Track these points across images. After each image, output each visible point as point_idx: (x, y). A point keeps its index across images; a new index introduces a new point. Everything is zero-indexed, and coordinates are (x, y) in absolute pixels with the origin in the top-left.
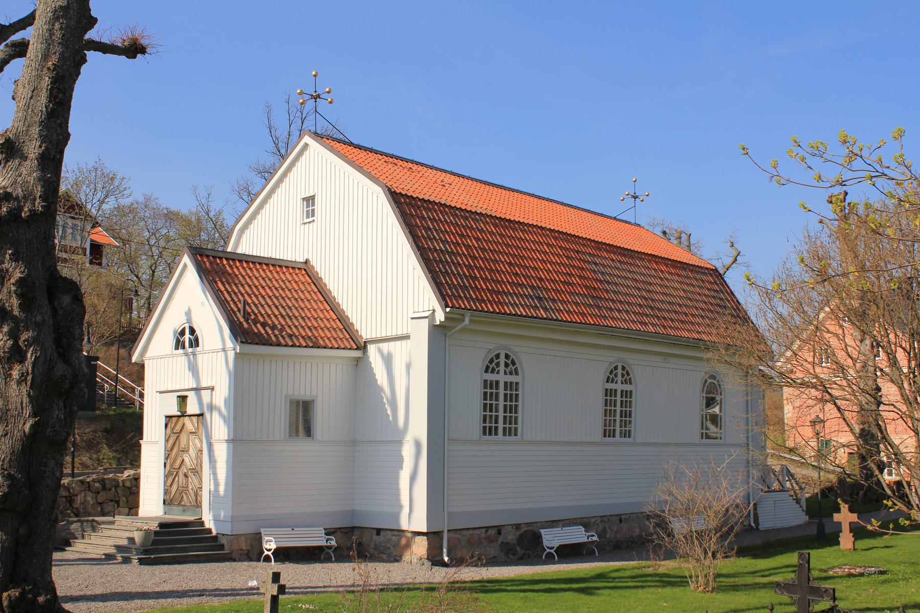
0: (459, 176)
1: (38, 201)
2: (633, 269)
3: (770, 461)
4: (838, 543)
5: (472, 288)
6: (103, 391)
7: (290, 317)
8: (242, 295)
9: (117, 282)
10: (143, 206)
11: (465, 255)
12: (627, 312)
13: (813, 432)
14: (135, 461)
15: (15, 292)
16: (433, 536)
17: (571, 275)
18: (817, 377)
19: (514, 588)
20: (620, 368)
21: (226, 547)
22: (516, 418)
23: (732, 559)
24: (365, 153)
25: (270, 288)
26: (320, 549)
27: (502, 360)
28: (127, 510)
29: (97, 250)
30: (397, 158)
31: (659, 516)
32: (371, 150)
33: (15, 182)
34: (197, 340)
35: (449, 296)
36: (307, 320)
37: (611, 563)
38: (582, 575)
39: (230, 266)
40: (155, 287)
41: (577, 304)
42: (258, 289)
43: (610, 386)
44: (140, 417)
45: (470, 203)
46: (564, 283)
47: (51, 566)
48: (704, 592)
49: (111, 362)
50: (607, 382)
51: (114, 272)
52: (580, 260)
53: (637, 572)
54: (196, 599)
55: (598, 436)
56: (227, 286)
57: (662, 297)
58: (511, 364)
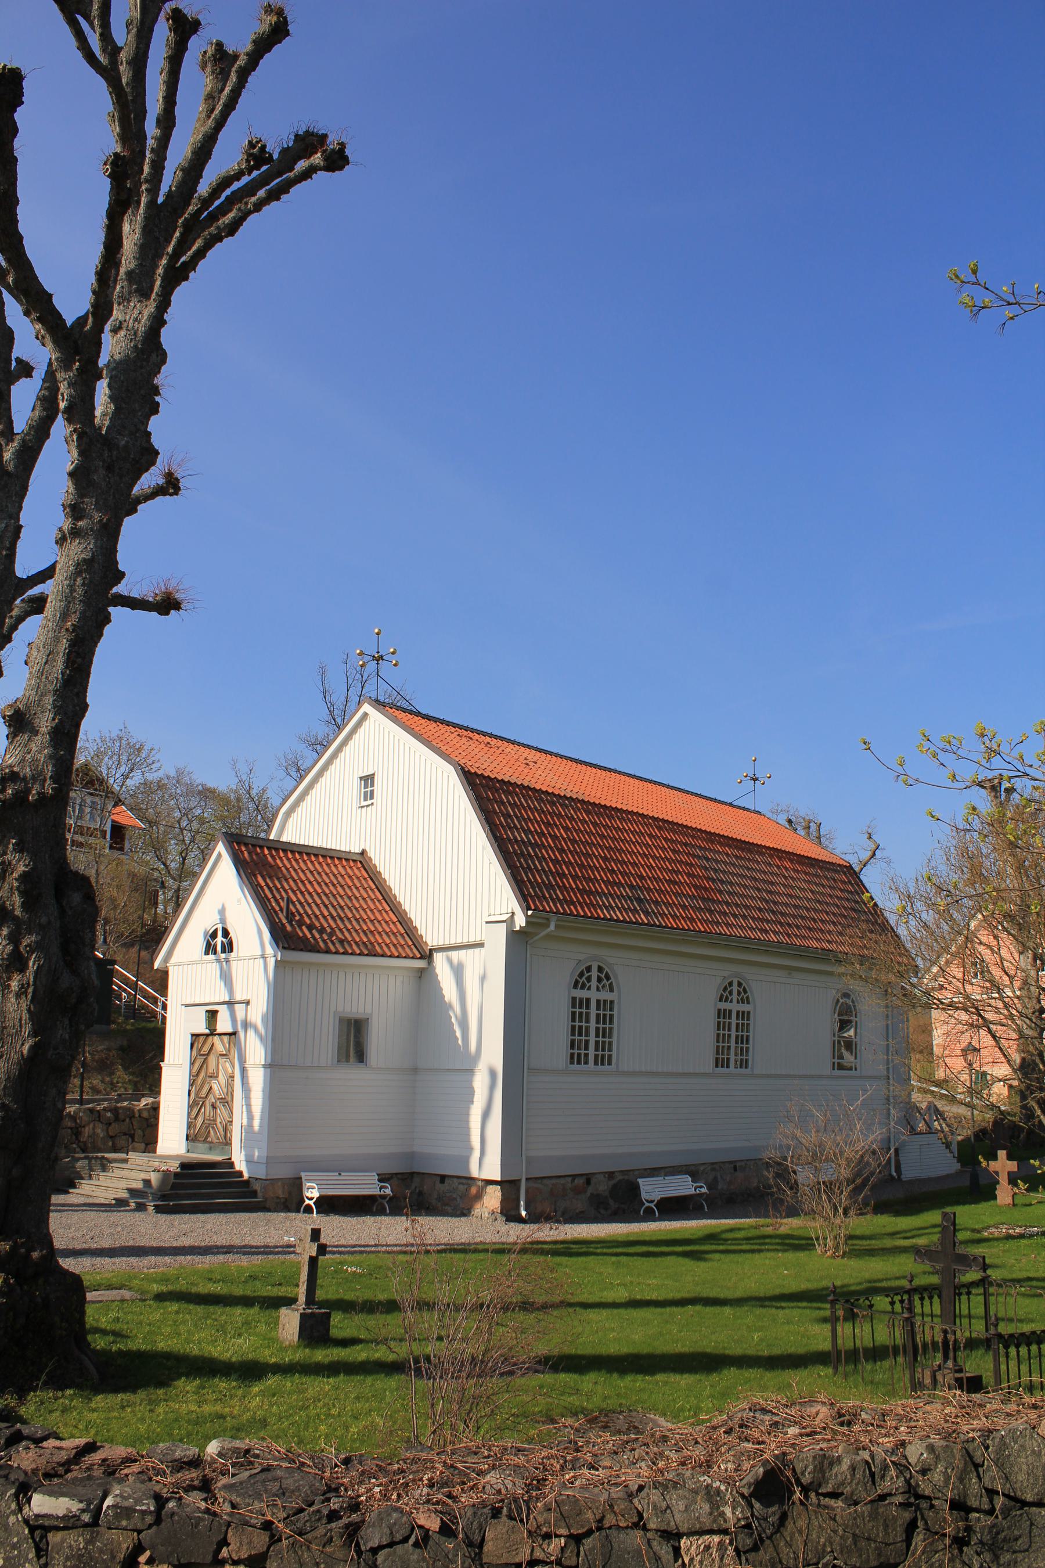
0: (546, 752)
1: (48, 782)
2: (751, 865)
3: (916, 1097)
4: (995, 1198)
5: (559, 887)
6: (120, 1001)
7: (341, 919)
8: (286, 891)
9: (141, 870)
10: (174, 782)
11: (551, 848)
12: (744, 917)
13: (970, 1062)
14: (154, 1086)
15: (18, 888)
16: (508, 1186)
17: (677, 872)
18: (967, 997)
19: (605, 1250)
20: (735, 984)
21: (260, 1194)
22: (610, 1043)
23: (868, 1217)
24: (434, 725)
25: (319, 883)
26: (372, 1198)
27: (594, 973)
28: (143, 1146)
29: (118, 832)
30: (473, 731)
31: (779, 1164)
32: (443, 722)
33: (23, 760)
34: (231, 943)
35: (531, 896)
36: (361, 922)
37: (723, 1221)
38: (687, 1236)
39: (272, 856)
40: (186, 877)
41: (684, 907)
42: (305, 885)
43: (723, 1005)
44: (160, 1034)
45: (558, 786)
46: (669, 882)
47: (49, 1211)
48: (833, 1257)
49: (130, 966)
50: (720, 1000)
51: (139, 859)
52: (688, 854)
53: (753, 1233)
54: (221, 1257)
55: (709, 1066)
56: (268, 880)
57: (785, 899)
58: (605, 978)
